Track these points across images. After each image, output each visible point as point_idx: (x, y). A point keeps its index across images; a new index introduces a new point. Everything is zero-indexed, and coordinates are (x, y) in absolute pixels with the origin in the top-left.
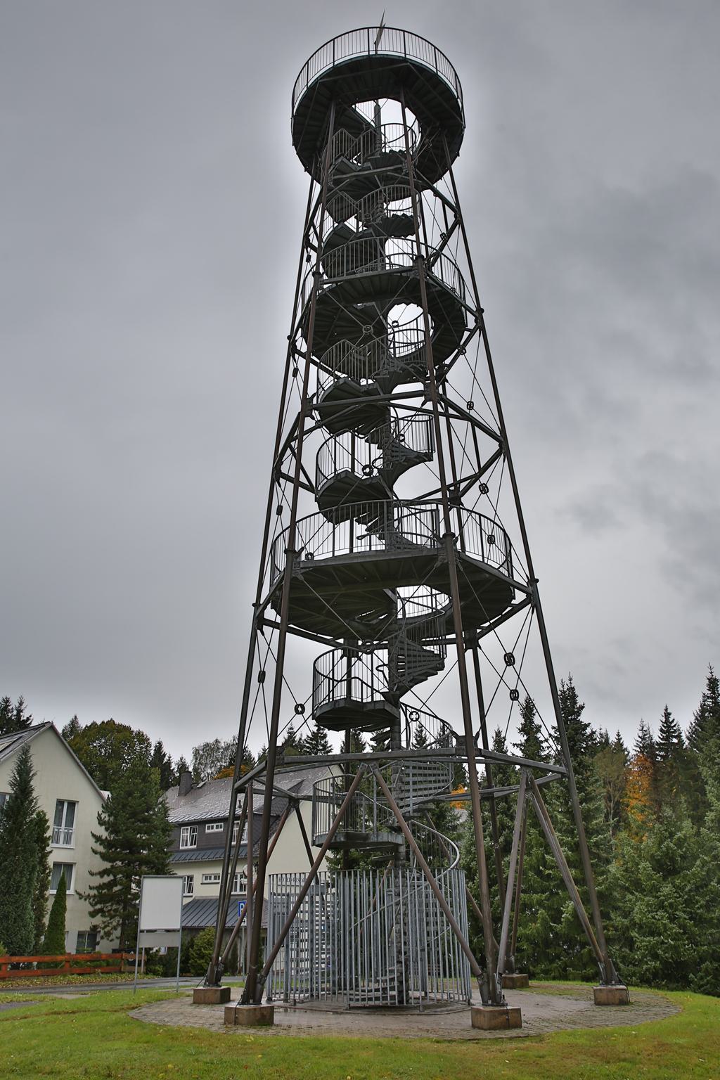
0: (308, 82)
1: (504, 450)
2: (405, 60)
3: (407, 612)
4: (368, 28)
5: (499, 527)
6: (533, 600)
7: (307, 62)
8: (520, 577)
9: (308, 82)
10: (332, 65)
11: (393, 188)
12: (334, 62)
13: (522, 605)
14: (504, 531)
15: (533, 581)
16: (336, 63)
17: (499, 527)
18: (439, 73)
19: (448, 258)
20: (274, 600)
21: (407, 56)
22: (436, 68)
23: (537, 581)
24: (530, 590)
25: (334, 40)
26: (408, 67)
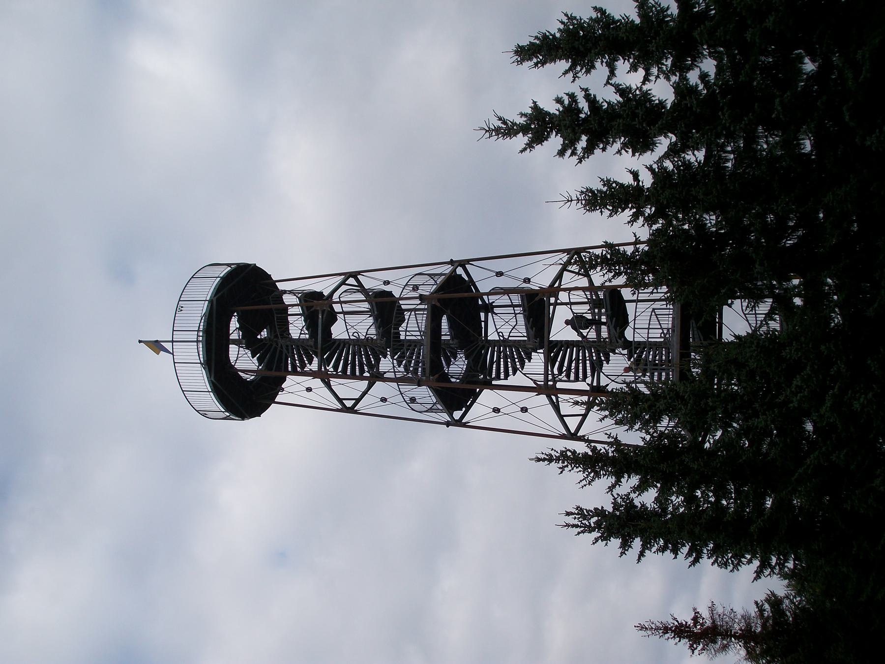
0: (222, 411)
1: (355, 275)
2: (211, 302)
3: (299, 313)
4: (174, 363)
5: (413, 277)
6: (463, 264)
7: (197, 411)
8: (447, 269)
9: (222, 411)
10: (211, 394)
11: (394, 341)
12: (209, 392)
13: (358, 281)
14: (416, 275)
15: (452, 262)
16: (210, 390)
17: (413, 277)
18: (221, 275)
19: (410, 280)
20: (450, 411)
21: (208, 299)
22: (217, 277)
23: (452, 260)
24: (456, 264)
25: (183, 391)
26: (217, 300)
